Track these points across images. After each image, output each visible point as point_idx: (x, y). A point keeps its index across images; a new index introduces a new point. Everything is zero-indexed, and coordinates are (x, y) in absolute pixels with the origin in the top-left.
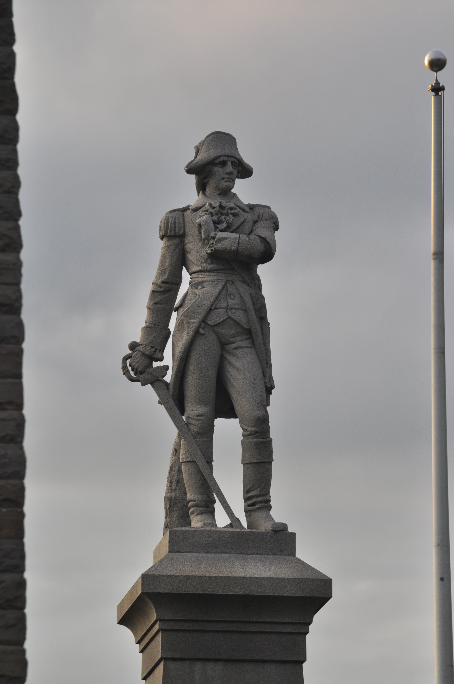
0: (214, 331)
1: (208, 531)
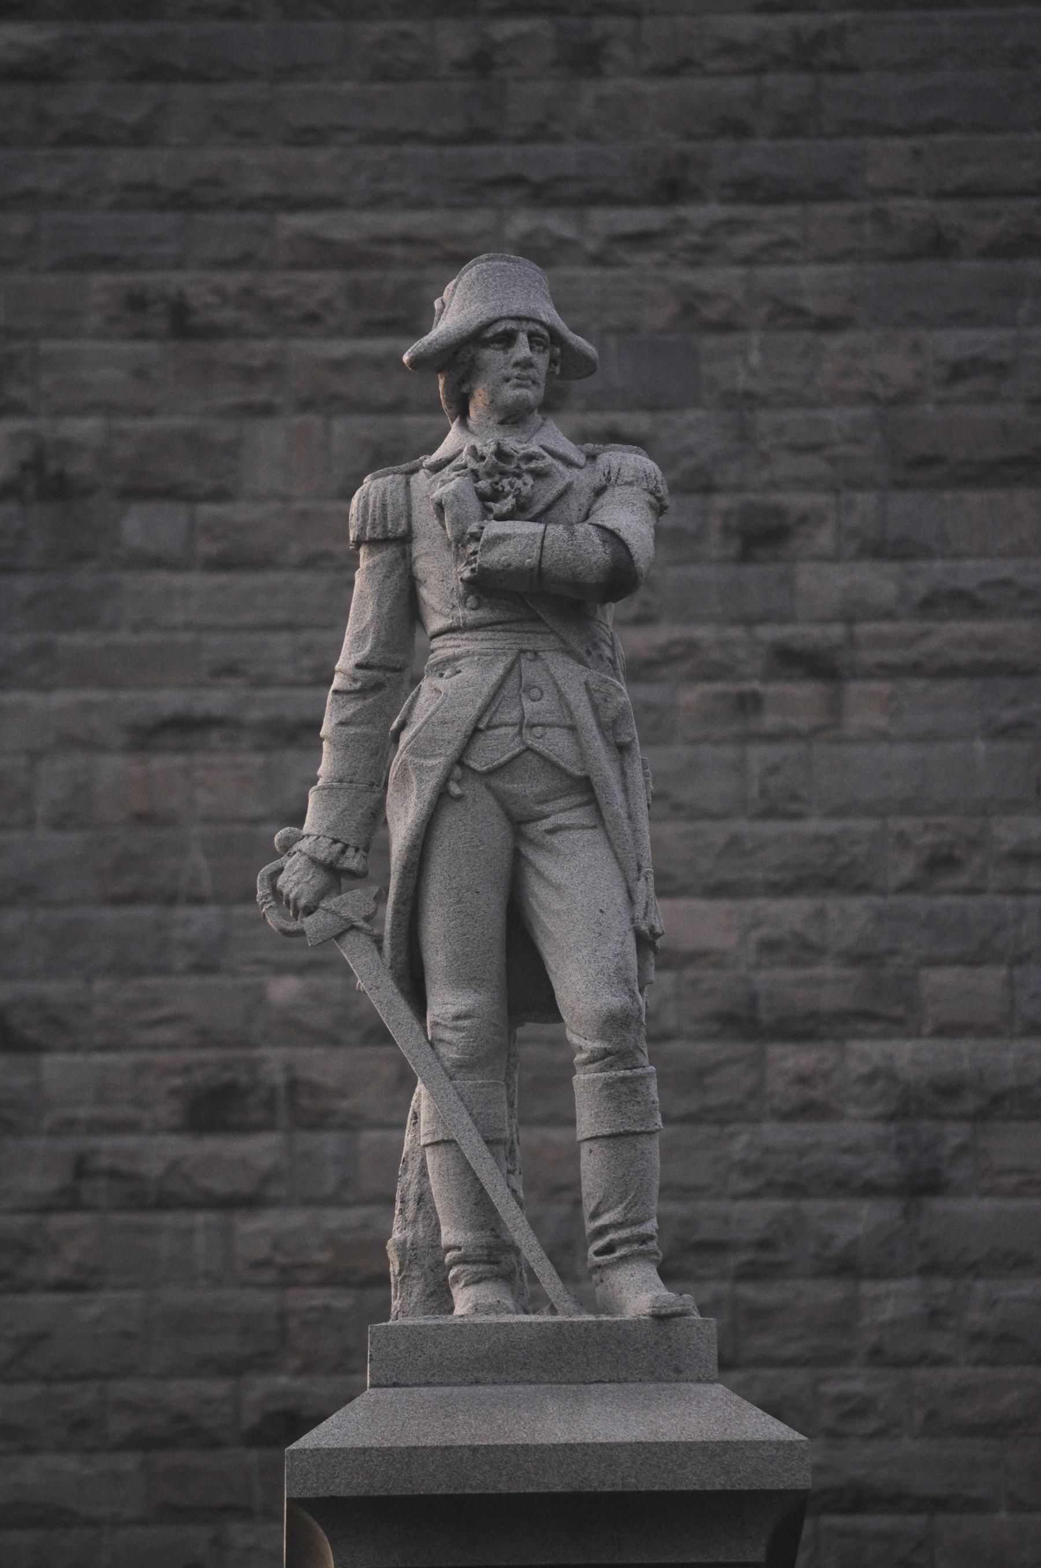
0: (489, 787)
1: (476, 1325)
